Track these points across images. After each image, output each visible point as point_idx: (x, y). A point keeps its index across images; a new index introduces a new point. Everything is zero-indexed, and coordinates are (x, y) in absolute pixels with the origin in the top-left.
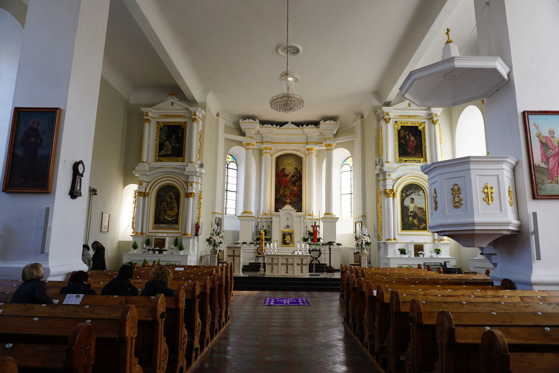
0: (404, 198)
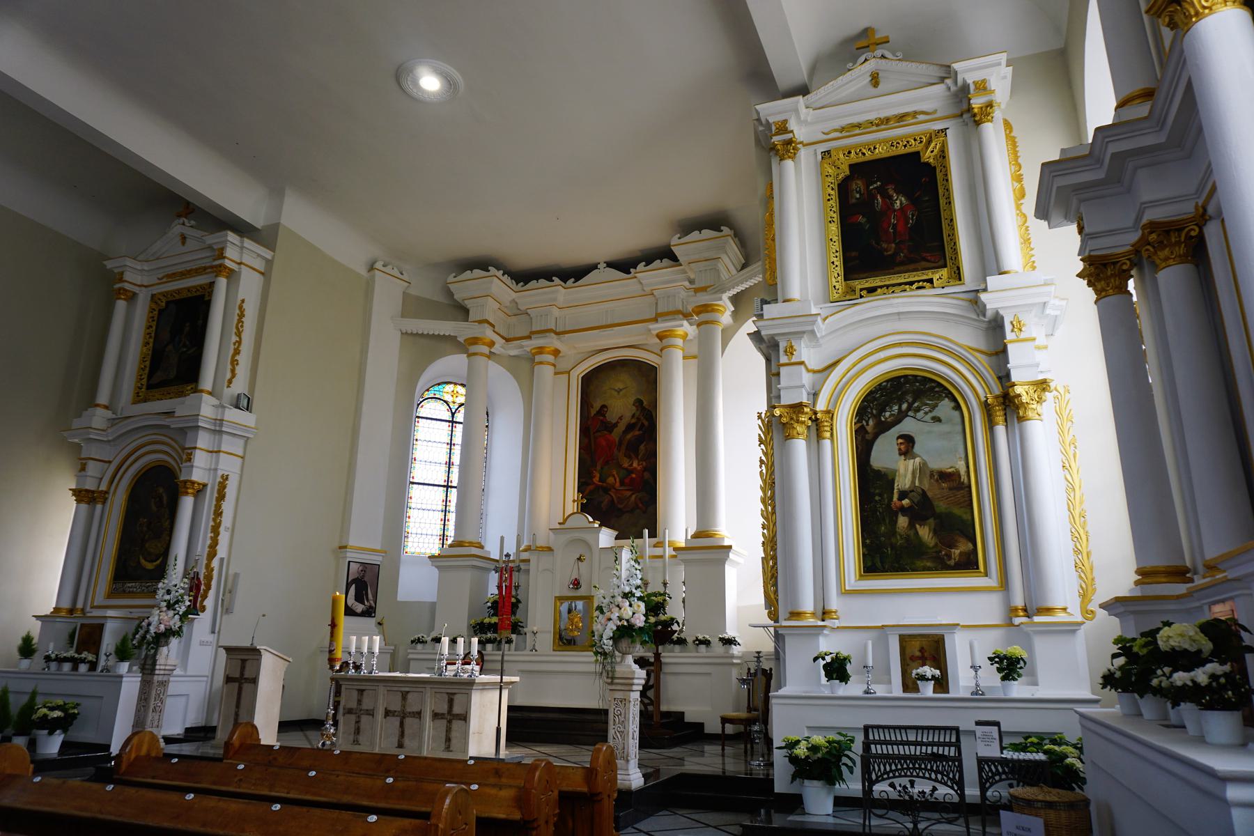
0: (869, 437)
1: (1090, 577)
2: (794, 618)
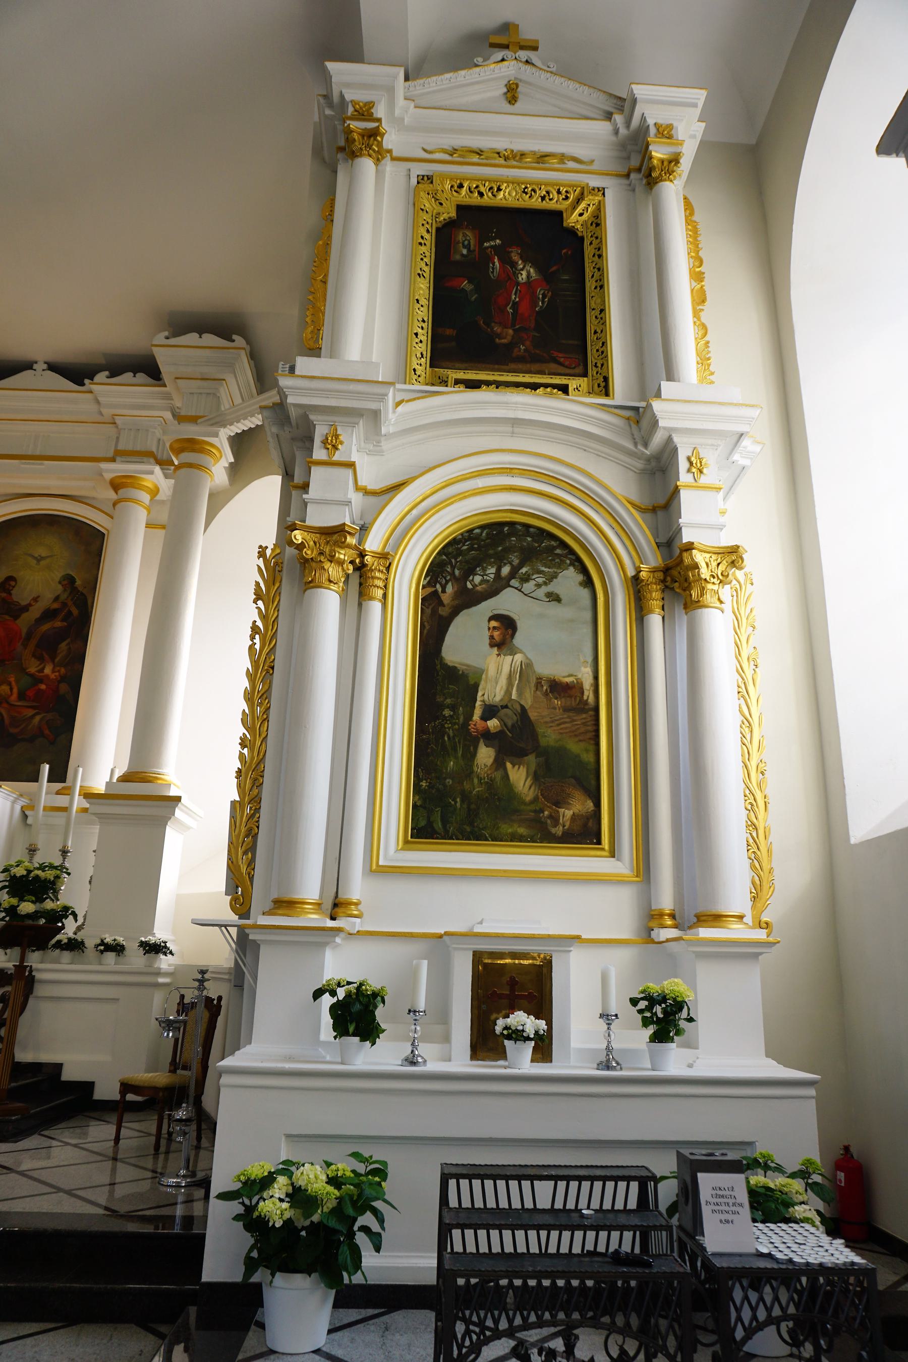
0: (443, 612)
1: (766, 866)
2: (280, 912)
